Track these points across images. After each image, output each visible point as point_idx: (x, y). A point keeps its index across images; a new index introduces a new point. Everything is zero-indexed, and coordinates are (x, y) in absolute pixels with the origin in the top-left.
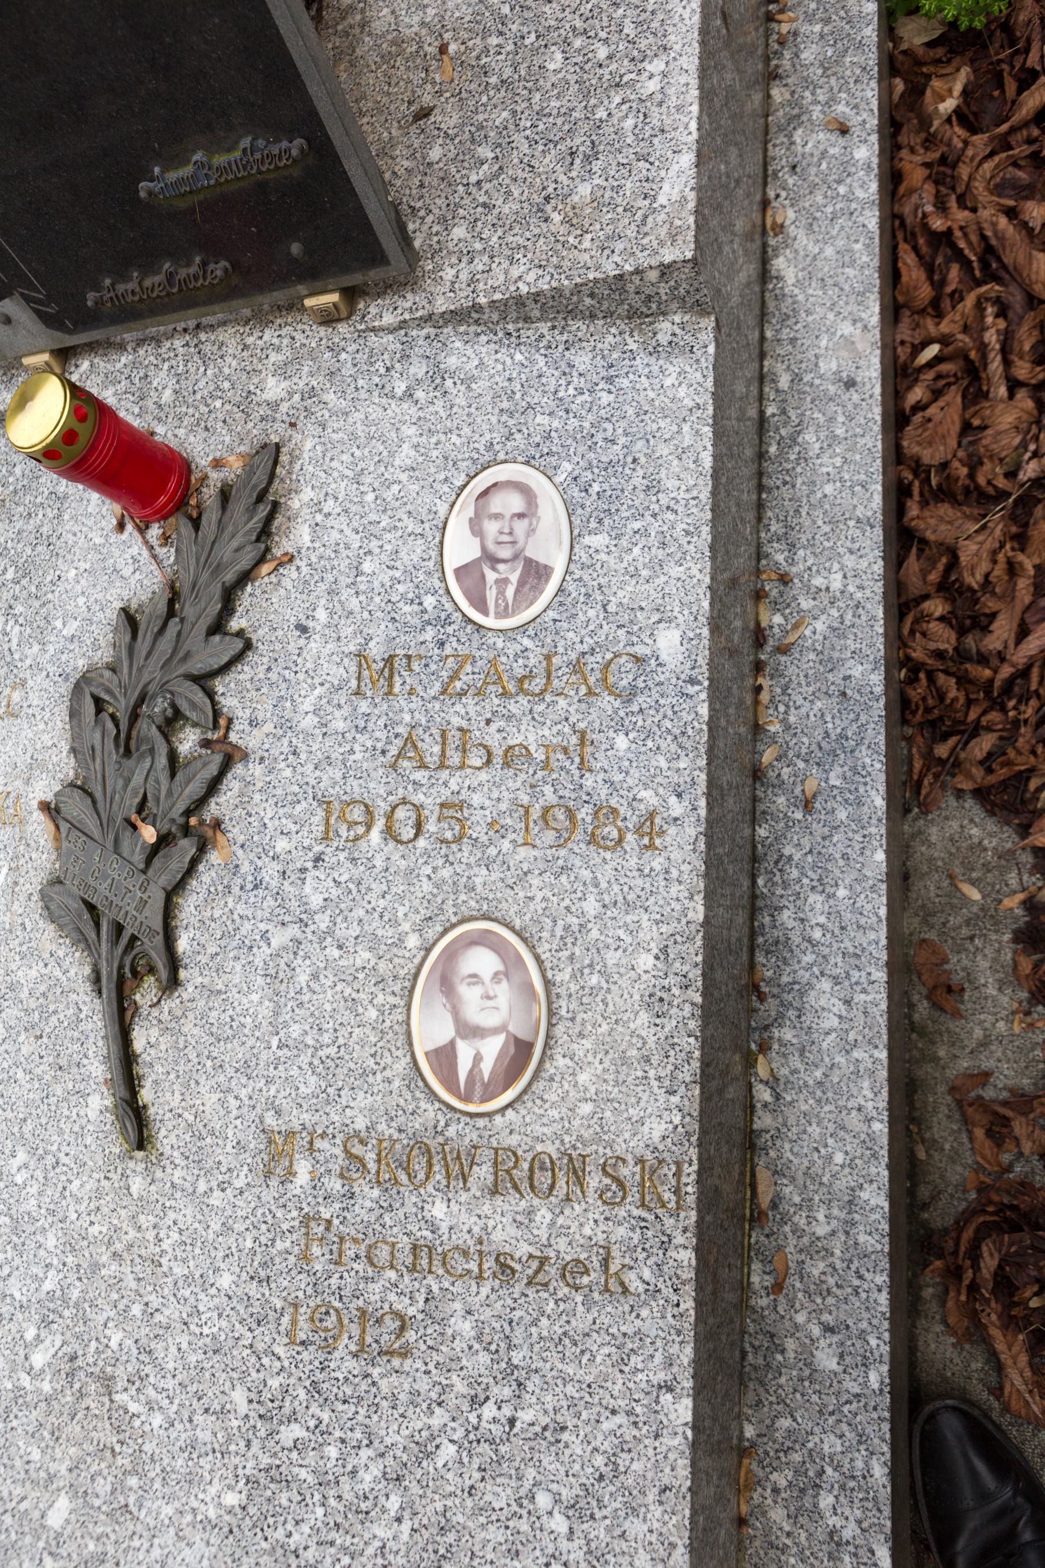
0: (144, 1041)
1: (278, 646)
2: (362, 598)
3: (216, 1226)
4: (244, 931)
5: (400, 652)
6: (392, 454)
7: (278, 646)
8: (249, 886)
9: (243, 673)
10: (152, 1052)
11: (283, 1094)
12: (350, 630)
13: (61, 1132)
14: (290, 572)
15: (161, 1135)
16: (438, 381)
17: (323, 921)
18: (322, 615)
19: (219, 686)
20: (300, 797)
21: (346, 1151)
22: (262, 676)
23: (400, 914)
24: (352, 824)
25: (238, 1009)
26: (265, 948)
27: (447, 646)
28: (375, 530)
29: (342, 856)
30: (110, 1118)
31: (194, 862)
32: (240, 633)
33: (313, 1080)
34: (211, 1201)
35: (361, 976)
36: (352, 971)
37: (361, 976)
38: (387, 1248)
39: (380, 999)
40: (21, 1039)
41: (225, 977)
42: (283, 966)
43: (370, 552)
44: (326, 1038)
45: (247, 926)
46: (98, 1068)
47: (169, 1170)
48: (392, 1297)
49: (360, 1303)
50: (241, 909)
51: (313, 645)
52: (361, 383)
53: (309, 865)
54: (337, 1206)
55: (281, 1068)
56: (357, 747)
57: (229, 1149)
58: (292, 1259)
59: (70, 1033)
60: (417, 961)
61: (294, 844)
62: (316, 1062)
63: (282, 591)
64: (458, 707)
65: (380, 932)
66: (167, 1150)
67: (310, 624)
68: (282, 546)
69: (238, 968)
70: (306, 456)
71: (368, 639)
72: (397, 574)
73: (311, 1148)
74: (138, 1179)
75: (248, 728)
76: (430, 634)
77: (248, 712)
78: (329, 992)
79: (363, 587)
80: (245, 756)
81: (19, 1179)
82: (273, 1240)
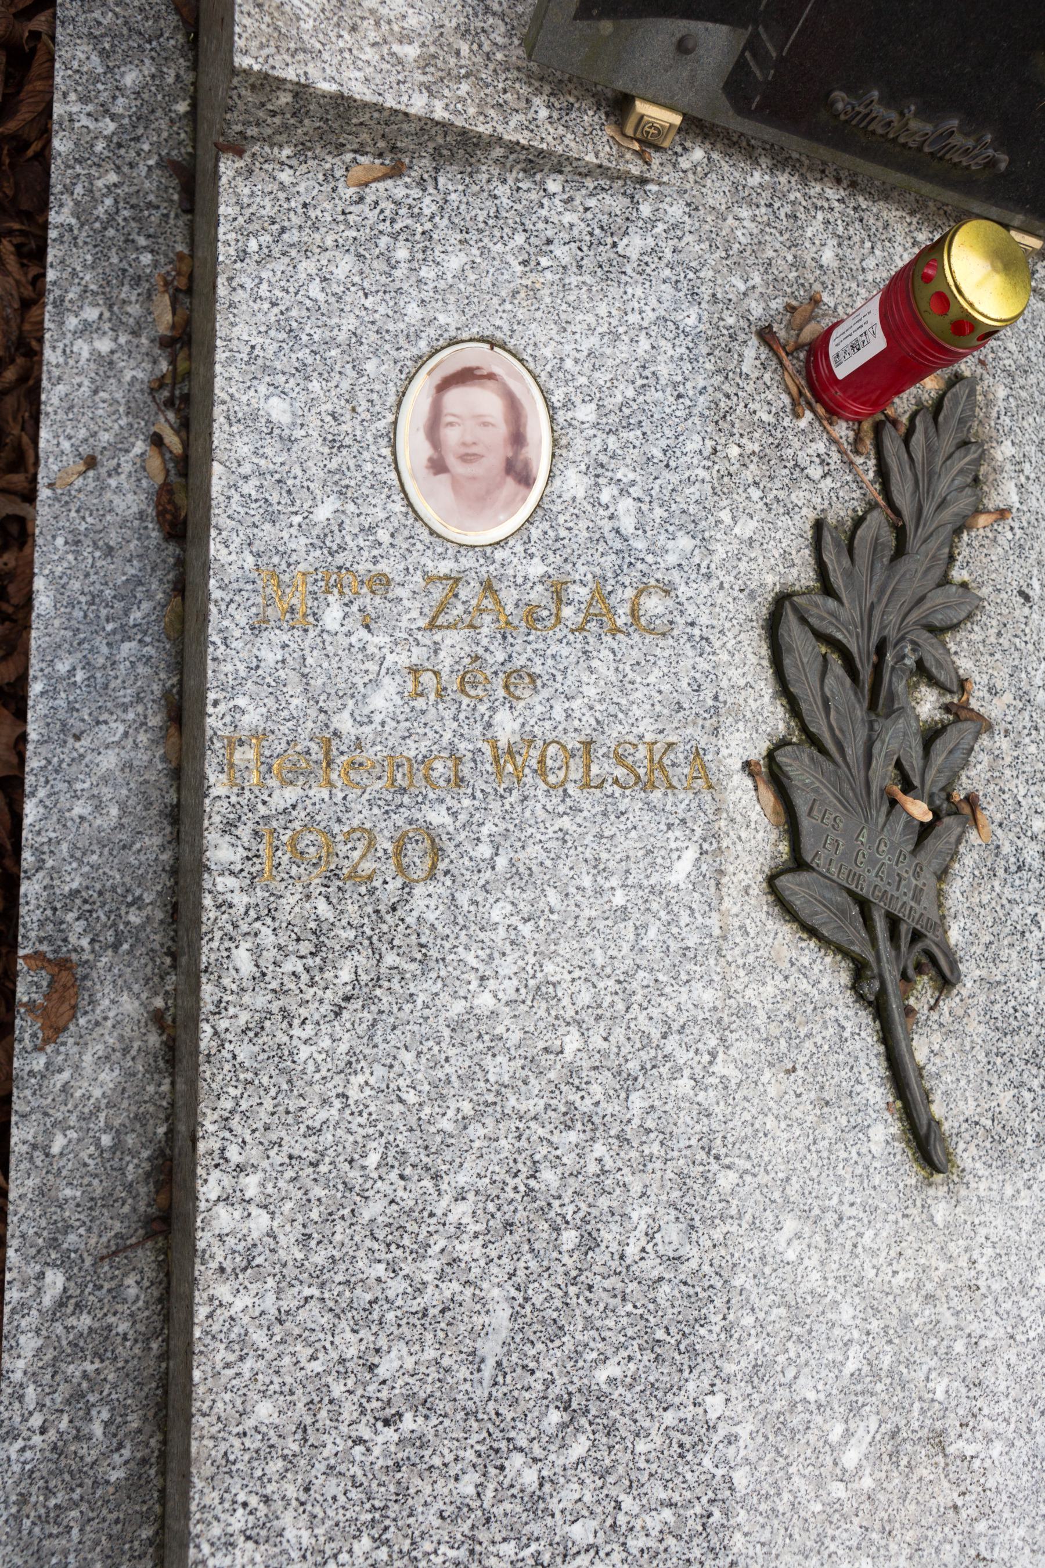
0: (926, 1051)
1: (1005, 611)
7: (1005, 611)
8: (1013, 868)
13: (840, 1180)
15: (959, 1151)
22: (993, 639)
26: (1036, 932)
30: (899, 1146)
32: (964, 585)
34: (1021, 1203)
46: (876, 1092)
47: (973, 1185)
50: (1008, 893)
57: (1030, 1144)
59: (833, 1059)
63: (1000, 550)
66: (968, 1164)
68: (994, 501)
70: (1001, 404)
74: (943, 1205)
75: (987, 696)
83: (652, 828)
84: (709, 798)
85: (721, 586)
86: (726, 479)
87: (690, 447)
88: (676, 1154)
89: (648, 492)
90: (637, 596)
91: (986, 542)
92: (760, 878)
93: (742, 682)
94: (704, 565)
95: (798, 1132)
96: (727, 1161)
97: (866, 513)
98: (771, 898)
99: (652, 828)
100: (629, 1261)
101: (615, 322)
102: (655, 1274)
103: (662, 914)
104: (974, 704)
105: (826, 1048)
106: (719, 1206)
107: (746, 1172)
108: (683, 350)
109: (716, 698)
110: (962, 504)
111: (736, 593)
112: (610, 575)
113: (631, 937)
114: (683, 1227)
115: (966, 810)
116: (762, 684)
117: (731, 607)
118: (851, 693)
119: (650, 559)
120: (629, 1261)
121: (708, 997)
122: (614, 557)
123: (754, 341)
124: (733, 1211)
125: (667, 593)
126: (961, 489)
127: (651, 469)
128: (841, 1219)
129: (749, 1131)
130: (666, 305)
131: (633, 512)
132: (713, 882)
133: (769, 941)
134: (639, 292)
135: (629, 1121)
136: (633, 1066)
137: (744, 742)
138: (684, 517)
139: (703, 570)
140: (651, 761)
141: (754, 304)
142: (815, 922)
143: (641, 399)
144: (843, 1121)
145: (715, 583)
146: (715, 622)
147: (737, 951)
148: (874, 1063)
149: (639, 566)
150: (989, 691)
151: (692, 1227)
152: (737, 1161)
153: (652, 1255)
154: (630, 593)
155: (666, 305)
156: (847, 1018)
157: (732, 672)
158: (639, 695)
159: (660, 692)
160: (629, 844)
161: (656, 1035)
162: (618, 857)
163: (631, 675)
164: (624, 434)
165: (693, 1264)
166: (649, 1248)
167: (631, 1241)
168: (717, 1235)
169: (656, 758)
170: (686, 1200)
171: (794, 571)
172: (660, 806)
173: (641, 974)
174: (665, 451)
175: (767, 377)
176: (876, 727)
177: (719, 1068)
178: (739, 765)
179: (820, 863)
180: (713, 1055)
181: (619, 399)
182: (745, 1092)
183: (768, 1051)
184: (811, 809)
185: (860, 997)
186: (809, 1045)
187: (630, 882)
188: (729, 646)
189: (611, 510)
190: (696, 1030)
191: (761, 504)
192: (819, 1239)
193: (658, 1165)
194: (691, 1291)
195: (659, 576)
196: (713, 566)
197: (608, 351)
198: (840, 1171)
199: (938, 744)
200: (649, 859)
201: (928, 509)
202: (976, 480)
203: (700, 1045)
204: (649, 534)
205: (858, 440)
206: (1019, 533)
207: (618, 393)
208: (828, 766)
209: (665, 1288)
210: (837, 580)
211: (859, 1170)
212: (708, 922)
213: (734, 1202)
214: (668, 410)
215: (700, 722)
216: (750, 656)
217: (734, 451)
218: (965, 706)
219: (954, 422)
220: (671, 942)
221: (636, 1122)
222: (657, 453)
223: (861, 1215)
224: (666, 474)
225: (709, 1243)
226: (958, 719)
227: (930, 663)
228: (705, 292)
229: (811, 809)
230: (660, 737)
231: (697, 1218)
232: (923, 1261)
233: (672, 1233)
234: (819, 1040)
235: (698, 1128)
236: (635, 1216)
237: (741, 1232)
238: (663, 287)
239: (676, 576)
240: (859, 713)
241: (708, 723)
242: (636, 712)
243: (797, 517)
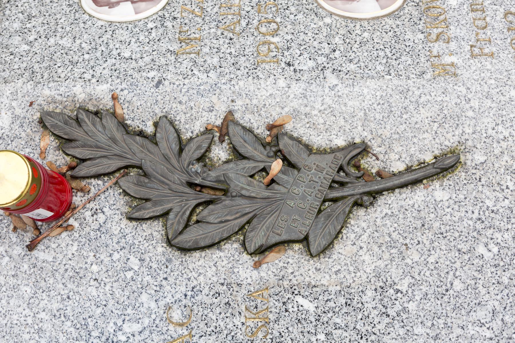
0: (399, 163)
1: (167, 98)
2: (145, 55)
3: (488, 103)
4: (330, 102)
5: (177, 36)
6: (63, 48)
7: (167, 98)
8: (305, 101)
9: (181, 119)
10: (404, 156)
11: (413, 71)
12: (162, 59)
13: (461, 219)
14: (124, 95)
15: (449, 144)
16: (26, 30)
17: (321, 60)
18: (151, 74)
19: (186, 136)
20: (255, 76)
21: (436, 41)
22: (184, 107)
23: (315, 26)
24: (270, 50)
25: (373, 101)
26: (338, 88)
27: (176, 16)
28: (106, 52)
29: (286, 53)
30: (446, 182)
31: (291, 138)
32: (156, 125)
33: (403, 58)
34: (477, 107)
35: (348, 41)
36: (346, 45)
37: (348, 41)
38: (476, 22)
39: (359, 32)
40: (409, 261)
41: (357, 112)
42: (347, 76)
43: (119, 54)
44: (382, 54)
45: (328, 100)
46: (418, 196)
47: (467, 137)
48: (498, 18)
49: (505, 30)
50: (318, 106)
51: (169, 77)
52: (16, 67)
53: (292, 68)
54: (463, 43)
55: (400, 73)
56: (228, 51)
57: (447, 99)
58: (494, 61)
59: (401, 221)
60: (337, 18)
61: (281, 77)
62: (394, 57)
63: (135, 99)
64: (209, 9)
65: (325, 34)
66: (456, 138)
67: (156, 80)
68: (107, 103)
69: (350, 103)
70: (53, 93)
71: (169, 50)
72: (133, 40)
73: (439, 56)
74: (476, 157)
75: (214, 113)
76: (169, 24)
77: (204, 113)
78: (358, 54)
79: (139, 55)
80: (231, 113)
81: (495, 250)
82: (488, 70)
83: (288, 319)
84: (272, 290)
85: (166, 279)
86: (110, 273)
87: (94, 293)
88: (444, 311)
89: (119, 316)
90: (173, 323)
91: (131, 108)
92: (312, 262)
93: (214, 269)
94: (155, 288)
95: (436, 243)
96: (449, 285)
97: (120, 187)
98: (322, 256)
99: (288, 319)
100: (493, 336)
101: (32, 331)
102: (500, 323)
103: (329, 315)
104: (219, 122)
105: (396, 225)
106: (470, 290)
107: (454, 274)
108: (44, 294)
109: (222, 284)
110: (110, 123)
111: (169, 270)
112: (162, 337)
113: (340, 331)
114: (479, 308)
115: (275, 131)
116: (214, 256)
117: (176, 274)
118: (217, 206)
119: (153, 316)
120: (493, 336)
121: (370, 293)
122: (153, 335)
123: (35, 252)
124: (473, 282)
125: (170, 308)
126: (104, 127)
127: (107, 314)
128: (479, 219)
129: (435, 272)
130: (22, 304)
131: (130, 324)
132: (314, 289)
133: (343, 257)
134: (15, 317)
135: (428, 334)
136: (402, 332)
137: (245, 270)
138: (131, 298)
139: (158, 289)
140: (254, 318)
141: (15, 252)
142: (334, 233)
143: (71, 318)
144: (432, 216)
145: (164, 283)
146: (184, 283)
147: (348, 277)
148: (404, 196)
149: (157, 322)
150: (211, 111)
151: (479, 304)
152: (449, 280)
153: (491, 324)
154: (171, 327)
155: (22, 304)
156: (381, 212)
157: (209, 274)
158: (222, 324)
159: (220, 313)
160: (295, 331)
161: (387, 320)
162: (302, 337)
163: (213, 328)
164: (91, 327)
165: (497, 303)
166: (487, 326)
167: (484, 334)
168: (483, 291)
169: (253, 316)
170: (466, 307)
171: (155, 234)
172: (277, 315)
173: (358, 327)
174: (98, 307)
175: (54, 246)
176: (234, 194)
177: (404, 289)
178: (255, 272)
179: (304, 231)
180: (398, 291)
181: (72, 329)
182: (416, 274)
183: (397, 260)
184: (278, 234)
185: (372, 204)
186: (395, 235)
187: (314, 332)
188: (196, 276)
189: (130, 335)
190: (386, 300)
191: (121, 253)
192: (489, 232)
193: (449, 320)
194: (509, 305)
195: (162, 312)
196: (156, 283)
197: (48, 334)
198: (456, 219)
199: (242, 151)
200: (303, 322)
201: (116, 150)
202: (96, 113)
203: (393, 298)
204: (141, 316)
205: (82, 190)
206: (124, 86)
207: (69, 331)
208: (255, 221)
209: (507, 318)
210: (159, 210)
211: (456, 207)
212: (333, 293)
213: (469, 282)
214: (76, 304)
215: (235, 293)
216: (200, 263)
217: (95, 268)
218: (220, 128)
219: (68, 129)
220: (343, 311)
221: (428, 331)
222: (99, 311)
223: (478, 207)
224: (110, 306)
225: (487, 295)
226: (227, 134)
227: (198, 154)
228: (12, 281)
229: (278, 234)
230: (243, 314)
231: (475, 301)
232: (502, 170)
233: (481, 314)
234: (392, 229)
235: (432, 300)
236: (472, 332)
237: (483, 278)
238: (12, 304)
239: (162, 303)
240: (227, 202)
241: (236, 289)
242: (230, 326)
243: (127, 231)
